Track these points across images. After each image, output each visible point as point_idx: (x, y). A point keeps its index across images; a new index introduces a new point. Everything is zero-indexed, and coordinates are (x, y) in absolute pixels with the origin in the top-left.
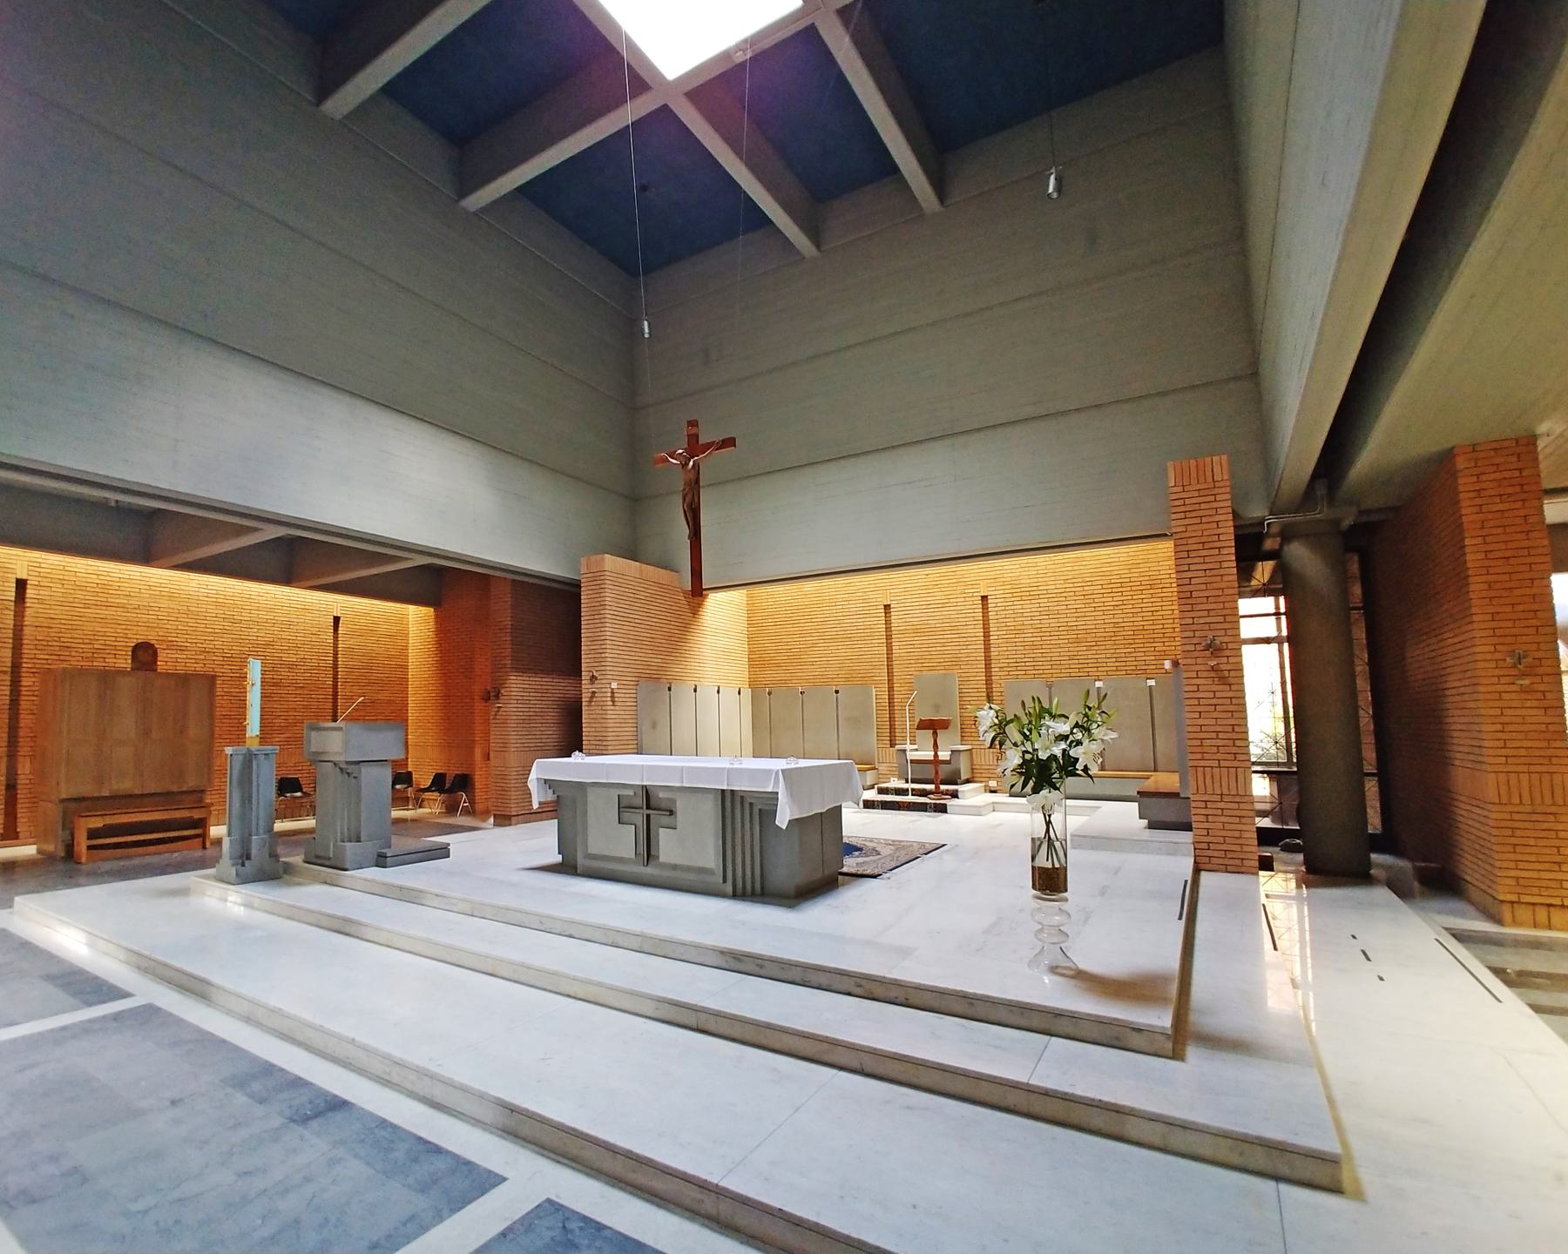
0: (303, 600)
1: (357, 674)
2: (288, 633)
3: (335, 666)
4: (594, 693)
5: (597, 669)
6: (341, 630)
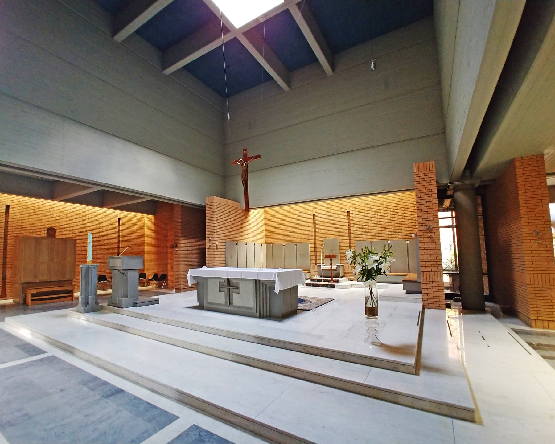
0: (107, 212)
1: (126, 239)
2: (102, 224)
3: (119, 236)
4: (210, 245)
5: (211, 237)
6: (121, 223)
